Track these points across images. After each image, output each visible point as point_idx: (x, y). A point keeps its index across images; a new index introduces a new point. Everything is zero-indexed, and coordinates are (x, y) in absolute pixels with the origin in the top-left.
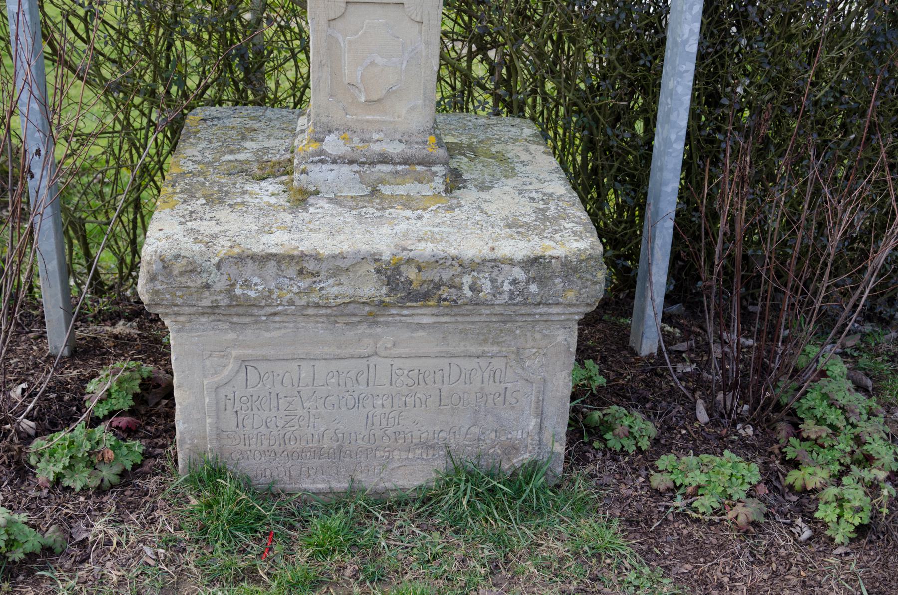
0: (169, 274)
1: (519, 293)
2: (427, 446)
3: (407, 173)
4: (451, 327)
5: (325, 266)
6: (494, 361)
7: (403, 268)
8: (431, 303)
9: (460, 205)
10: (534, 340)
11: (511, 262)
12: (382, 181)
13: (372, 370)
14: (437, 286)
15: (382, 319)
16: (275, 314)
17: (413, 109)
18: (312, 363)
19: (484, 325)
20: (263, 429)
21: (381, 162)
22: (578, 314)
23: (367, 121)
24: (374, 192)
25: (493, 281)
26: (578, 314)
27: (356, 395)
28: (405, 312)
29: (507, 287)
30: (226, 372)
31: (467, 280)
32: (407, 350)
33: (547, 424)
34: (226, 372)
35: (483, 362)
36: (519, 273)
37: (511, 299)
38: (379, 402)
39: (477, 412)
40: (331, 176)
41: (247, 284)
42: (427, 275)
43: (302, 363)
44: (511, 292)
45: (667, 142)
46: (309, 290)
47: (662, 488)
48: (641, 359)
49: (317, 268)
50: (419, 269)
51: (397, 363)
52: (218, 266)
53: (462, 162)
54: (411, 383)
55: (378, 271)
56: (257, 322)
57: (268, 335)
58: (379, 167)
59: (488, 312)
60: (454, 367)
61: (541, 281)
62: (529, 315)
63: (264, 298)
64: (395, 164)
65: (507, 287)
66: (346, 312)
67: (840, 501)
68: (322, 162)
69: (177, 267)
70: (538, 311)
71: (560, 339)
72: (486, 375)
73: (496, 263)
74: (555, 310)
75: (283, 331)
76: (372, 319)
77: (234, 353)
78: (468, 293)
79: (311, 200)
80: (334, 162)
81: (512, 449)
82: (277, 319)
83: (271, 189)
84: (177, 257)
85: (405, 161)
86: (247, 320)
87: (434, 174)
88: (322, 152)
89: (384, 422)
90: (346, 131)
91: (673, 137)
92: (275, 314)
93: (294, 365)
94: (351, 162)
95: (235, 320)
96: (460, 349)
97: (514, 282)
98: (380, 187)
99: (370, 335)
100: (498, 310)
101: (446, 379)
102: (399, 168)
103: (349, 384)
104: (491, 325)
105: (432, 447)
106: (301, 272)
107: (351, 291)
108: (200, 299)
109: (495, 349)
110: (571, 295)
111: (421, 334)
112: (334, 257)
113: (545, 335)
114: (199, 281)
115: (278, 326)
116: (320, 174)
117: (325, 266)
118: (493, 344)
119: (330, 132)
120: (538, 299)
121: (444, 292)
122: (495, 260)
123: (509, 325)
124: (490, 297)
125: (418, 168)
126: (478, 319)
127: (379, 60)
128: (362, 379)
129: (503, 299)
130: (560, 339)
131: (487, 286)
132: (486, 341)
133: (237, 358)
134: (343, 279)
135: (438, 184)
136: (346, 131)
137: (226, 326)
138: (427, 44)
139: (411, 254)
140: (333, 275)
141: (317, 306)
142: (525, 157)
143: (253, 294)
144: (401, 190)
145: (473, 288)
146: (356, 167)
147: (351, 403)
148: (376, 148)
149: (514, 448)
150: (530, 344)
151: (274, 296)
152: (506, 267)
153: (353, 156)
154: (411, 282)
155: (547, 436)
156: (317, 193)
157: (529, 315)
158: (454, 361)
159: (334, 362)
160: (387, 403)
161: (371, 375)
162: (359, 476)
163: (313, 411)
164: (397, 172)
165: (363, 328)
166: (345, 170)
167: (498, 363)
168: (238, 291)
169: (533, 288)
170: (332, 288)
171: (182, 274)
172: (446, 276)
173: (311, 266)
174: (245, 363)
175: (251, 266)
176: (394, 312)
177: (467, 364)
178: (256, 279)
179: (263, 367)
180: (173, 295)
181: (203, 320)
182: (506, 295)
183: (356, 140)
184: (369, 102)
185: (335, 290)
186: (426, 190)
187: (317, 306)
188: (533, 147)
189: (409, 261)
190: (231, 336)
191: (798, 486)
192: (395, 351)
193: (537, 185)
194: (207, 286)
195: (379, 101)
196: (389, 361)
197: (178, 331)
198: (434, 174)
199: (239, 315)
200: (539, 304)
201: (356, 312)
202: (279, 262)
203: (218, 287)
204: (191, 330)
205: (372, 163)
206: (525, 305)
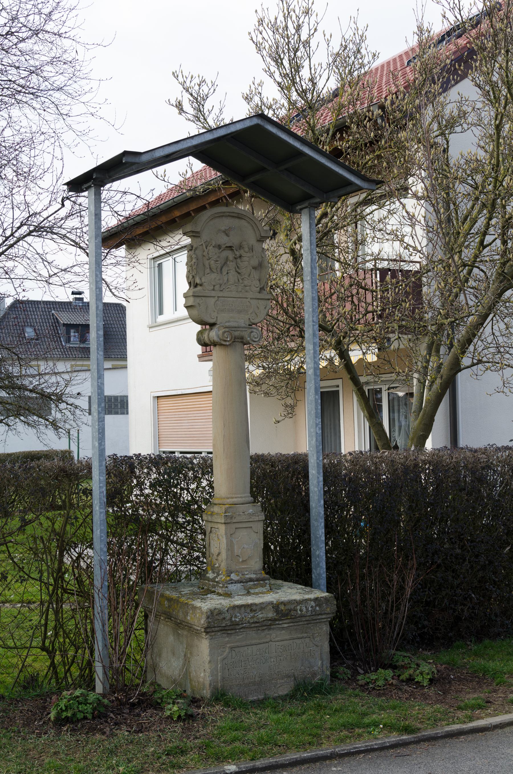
0: (213, 616)
2: (288, 676)
3: (258, 584)
5: (258, 607)
11: (310, 600)
12: (250, 588)
14: (290, 610)
17: (256, 562)
20: (237, 675)
25: (306, 607)
28: (281, 622)
29: (310, 609)
30: (225, 654)
31: (298, 608)
33: (324, 663)
34: (225, 654)
35: (303, 640)
36: (313, 604)
40: (235, 588)
42: (288, 607)
45: (319, 575)
46: (253, 617)
47: (363, 684)
50: (285, 605)
51: (277, 643)
52: (227, 611)
55: (273, 607)
56: (236, 632)
57: (238, 637)
58: (249, 583)
61: (320, 605)
65: (310, 609)
67: (421, 673)
68: (232, 583)
69: (216, 612)
74: (324, 616)
76: (269, 627)
77: (228, 645)
78: (299, 612)
80: (235, 583)
81: (314, 674)
84: (215, 609)
85: (258, 580)
86: (233, 631)
88: (232, 580)
90: (237, 572)
91: (322, 572)
93: (246, 648)
94: (241, 582)
95: (229, 632)
96: (295, 636)
97: (312, 607)
98: (250, 590)
100: (307, 618)
105: (289, 677)
106: (251, 610)
107: (265, 616)
109: (306, 635)
110: (328, 609)
111: (283, 632)
112: (260, 604)
114: (222, 617)
116: (232, 587)
117: (258, 607)
121: (293, 613)
127: (246, 546)
128: (267, 651)
132: (303, 632)
133: (229, 647)
136: (237, 572)
137: (225, 635)
138: (259, 539)
140: (260, 610)
141: (257, 622)
143: (237, 620)
148: (247, 576)
149: (315, 674)
152: (309, 602)
155: (324, 668)
158: (294, 641)
160: (275, 660)
162: (267, 692)
165: (266, 632)
167: (307, 640)
168: (233, 619)
169: (318, 608)
170: (260, 615)
171: (217, 615)
172: (292, 607)
173: (254, 608)
174: (232, 648)
175: (237, 610)
177: (298, 641)
178: (238, 615)
179: (236, 650)
180: (214, 623)
183: (240, 574)
184: (243, 561)
185: (261, 616)
186: (264, 590)
190: (227, 639)
191: (405, 679)
192: (276, 639)
205: (247, 582)
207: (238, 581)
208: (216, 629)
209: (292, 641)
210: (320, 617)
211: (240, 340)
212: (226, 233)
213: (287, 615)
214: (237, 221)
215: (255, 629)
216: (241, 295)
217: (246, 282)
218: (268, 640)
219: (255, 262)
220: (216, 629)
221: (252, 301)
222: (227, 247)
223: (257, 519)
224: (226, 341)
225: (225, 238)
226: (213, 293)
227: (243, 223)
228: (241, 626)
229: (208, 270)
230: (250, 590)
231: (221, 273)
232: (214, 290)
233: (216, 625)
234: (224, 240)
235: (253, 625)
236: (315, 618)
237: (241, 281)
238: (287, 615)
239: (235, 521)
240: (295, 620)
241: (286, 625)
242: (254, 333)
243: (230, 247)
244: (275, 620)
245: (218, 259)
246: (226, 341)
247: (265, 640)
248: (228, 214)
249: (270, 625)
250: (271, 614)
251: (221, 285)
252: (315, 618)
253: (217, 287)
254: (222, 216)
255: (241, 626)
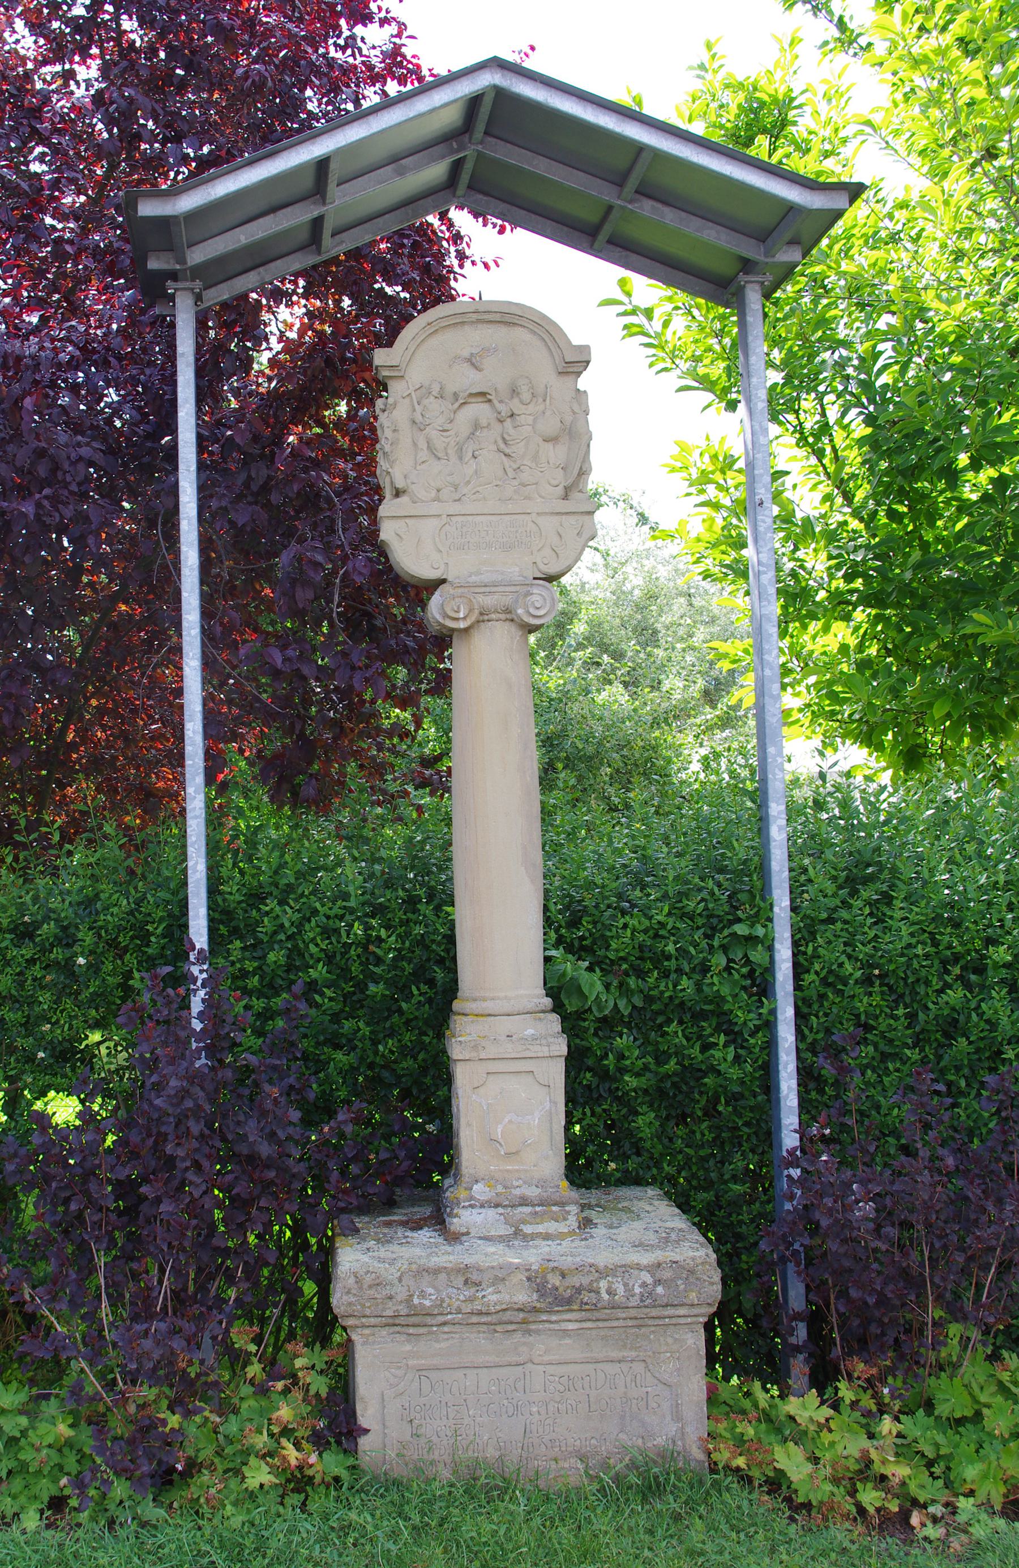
0: (361, 1288)
1: (648, 1295)
3: (545, 1213)
4: (594, 1332)
6: (634, 1365)
7: (550, 1276)
8: (575, 1307)
9: (592, 1237)
10: (667, 1344)
11: (639, 1267)
12: (524, 1222)
13: (528, 1377)
14: (579, 1290)
15: (533, 1327)
16: (444, 1324)
18: (475, 1371)
19: (621, 1330)
21: (521, 1205)
22: (702, 1315)
23: (508, 1171)
24: (517, 1233)
25: (626, 1285)
26: (702, 1315)
27: (514, 1402)
28: (554, 1318)
29: (637, 1290)
31: (603, 1285)
32: (557, 1357)
35: (625, 1367)
37: (642, 1301)
38: (535, 1409)
39: (623, 1418)
40: (479, 1219)
41: (423, 1295)
42: (575, 1281)
43: (468, 1371)
44: (642, 1295)
46: (471, 1300)
48: (421, 627)
49: (479, 1279)
51: (551, 1369)
53: (592, 1214)
54: (562, 1389)
55: (529, 1279)
56: (430, 1333)
57: (437, 1346)
58: (520, 1209)
59: (624, 1315)
60: (599, 1372)
62: (659, 1318)
63: (436, 1306)
64: (533, 1206)
65: (637, 1290)
66: (504, 1319)
68: (472, 1206)
69: (368, 1279)
70: (666, 1313)
71: (690, 1342)
72: (628, 1379)
73: (626, 1268)
74: (682, 1311)
75: (450, 1342)
78: (606, 1297)
79: (464, 1238)
80: (482, 1206)
82: (446, 1329)
83: (428, 1234)
86: (422, 1330)
87: (568, 1212)
89: (541, 1430)
92: (444, 1324)
93: (460, 1373)
94: (497, 1206)
95: (411, 1330)
97: (644, 1285)
98: (522, 1227)
99: (525, 1344)
100: (633, 1313)
101: (593, 1384)
102: (538, 1209)
103: (508, 1392)
104: (629, 1330)
106: (466, 1282)
107: (507, 1297)
108: (384, 1309)
109: (634, 1354)
111: (568, 1341)
113: (676, 1340)
115: (446, 1336)
118: (631, 1349)
119: (477, 1181)
120: (665, 1300)
122: (624, 1266)
123: (643, 1330)
124: (624, 1300)
125: (554, 1208)
126: (615, 1324)
128: (520, 1385)
129: (634, 1301)
130: (690, 1342)
131: (620, 1290)
132: (624, 1346)
134: (501, 1287)
135: (572, 1221)
137: (403, 1338)
139: (556, 1264)
141: (480, 1313)
142: (648, 1208)
143: (427, 1303)
144: (540, 1229)
145: (609, 1292)
146: (500, 1210)
147: (511, 1411)
148: (517, 1192)
150: (664, 1348)
151: (445, 1305)
153: (498, 1200)
154: (557, 1289)
156: (468, 1233)
157: (659, 1318)
159: (494, 1370)
161: (527, 1382)
163: (478, 1419)
164: (536, 1213)
165: (518, 1337)
166: (491, 1213)
168: (416, 1301)
170: (492, 1297)
171: (370, 1287)
172: (585, 1281)
173: (475, 1277)
176: (544, 1317)
177: (611, 1369)
178: (430, 1290)
181: (384, 1332)
182: (637, 1298)
185: (494, 1298)
186: (562, 1228)
187: (480, 1313)
188: (656, 1203)
189: (554, 1269)
190: (408, 1347)
192: (546, 1358)
193: (660, 1223)
194: (391, 1298)
195: (517, 1153)
196: (541, 1368)
197: (364, 1343)
198: (568, 1212)
199: (414, 1326)
200: (667, 1305)
201: (512, 1319)
202: (448, 1274)
203: (399, 1298)
204: (374, 1342)
206: (654, 1307)
207: (489, 1202)
208: (373, 1321)
209: (591, 1366)
210: (670, 1311)
211: (503, 616)
212: (473, 362)
213: (569, 1301)
214: (503, 330)
215: (484, 1328)
216: (510, 507)
217: (525, 476)
218: (521, 1359)
219: (550, 425)
220: (373, 1321)
221: (541, 521)
222: (471, 395)
223: (545, 1051)
224: (457, 619)
225: (472, 374)
226: (435, 508)
227: (519, 333)
228: (441, 1319)
229: (424, 454)
230: (522, 1227)
231: (461, 458)
232: (437, 499)
233: (368, 1312)
234: (468, 379)
235: (475, 1319)
236: (654, 1312)
237: (511, 473)
238: (569, 1301)
239: (483, 1056)
240: (597, 1315)
241: (571, 1326)
242: (534, 598)
243: (483, 394)
244: (535, 1310)
245: (447, 427)
246: (457, 619)
247: (515, 1359)
248: (475, 316)
249: (524, 1322)
250: (523, 1297)
251: (456, 488)
252: (654, 1312)
253: (445, 493)
254: (463, 323)
255: (441, 1319)
